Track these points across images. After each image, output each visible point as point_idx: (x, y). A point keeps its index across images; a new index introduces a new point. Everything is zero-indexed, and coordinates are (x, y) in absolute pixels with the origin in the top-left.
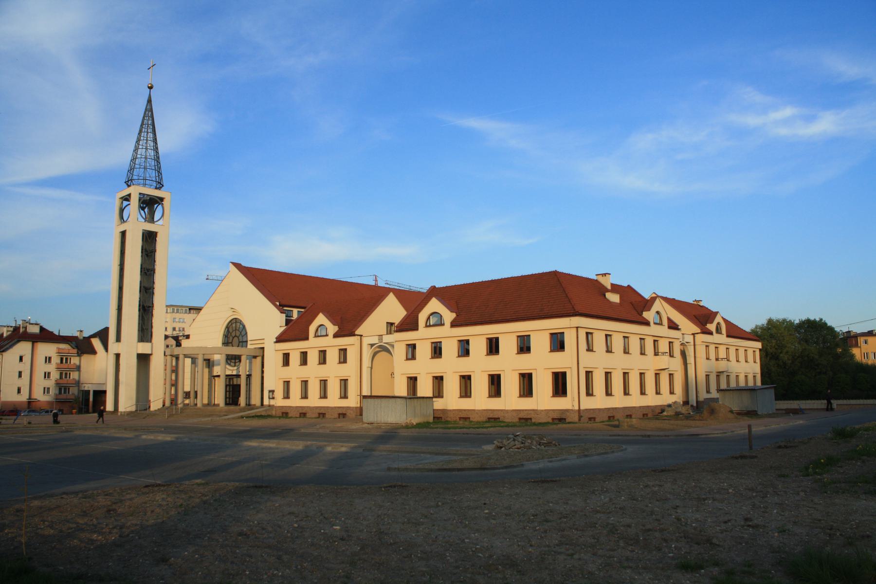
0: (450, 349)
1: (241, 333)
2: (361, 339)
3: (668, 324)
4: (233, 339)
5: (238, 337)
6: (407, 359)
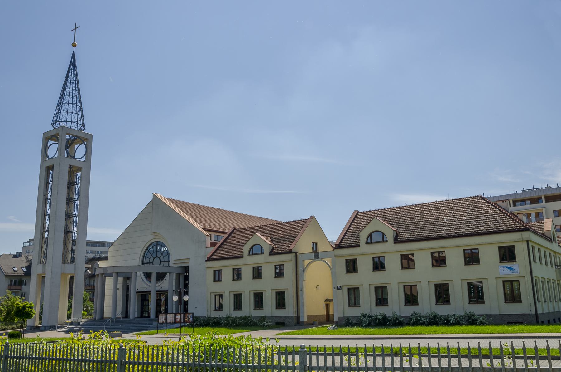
0: (268, 272)
1: (162, 254)
2: (521, 241)
3: (30, 279)
4: (154, 260)
5: (159, 258)
6: (234, 280)
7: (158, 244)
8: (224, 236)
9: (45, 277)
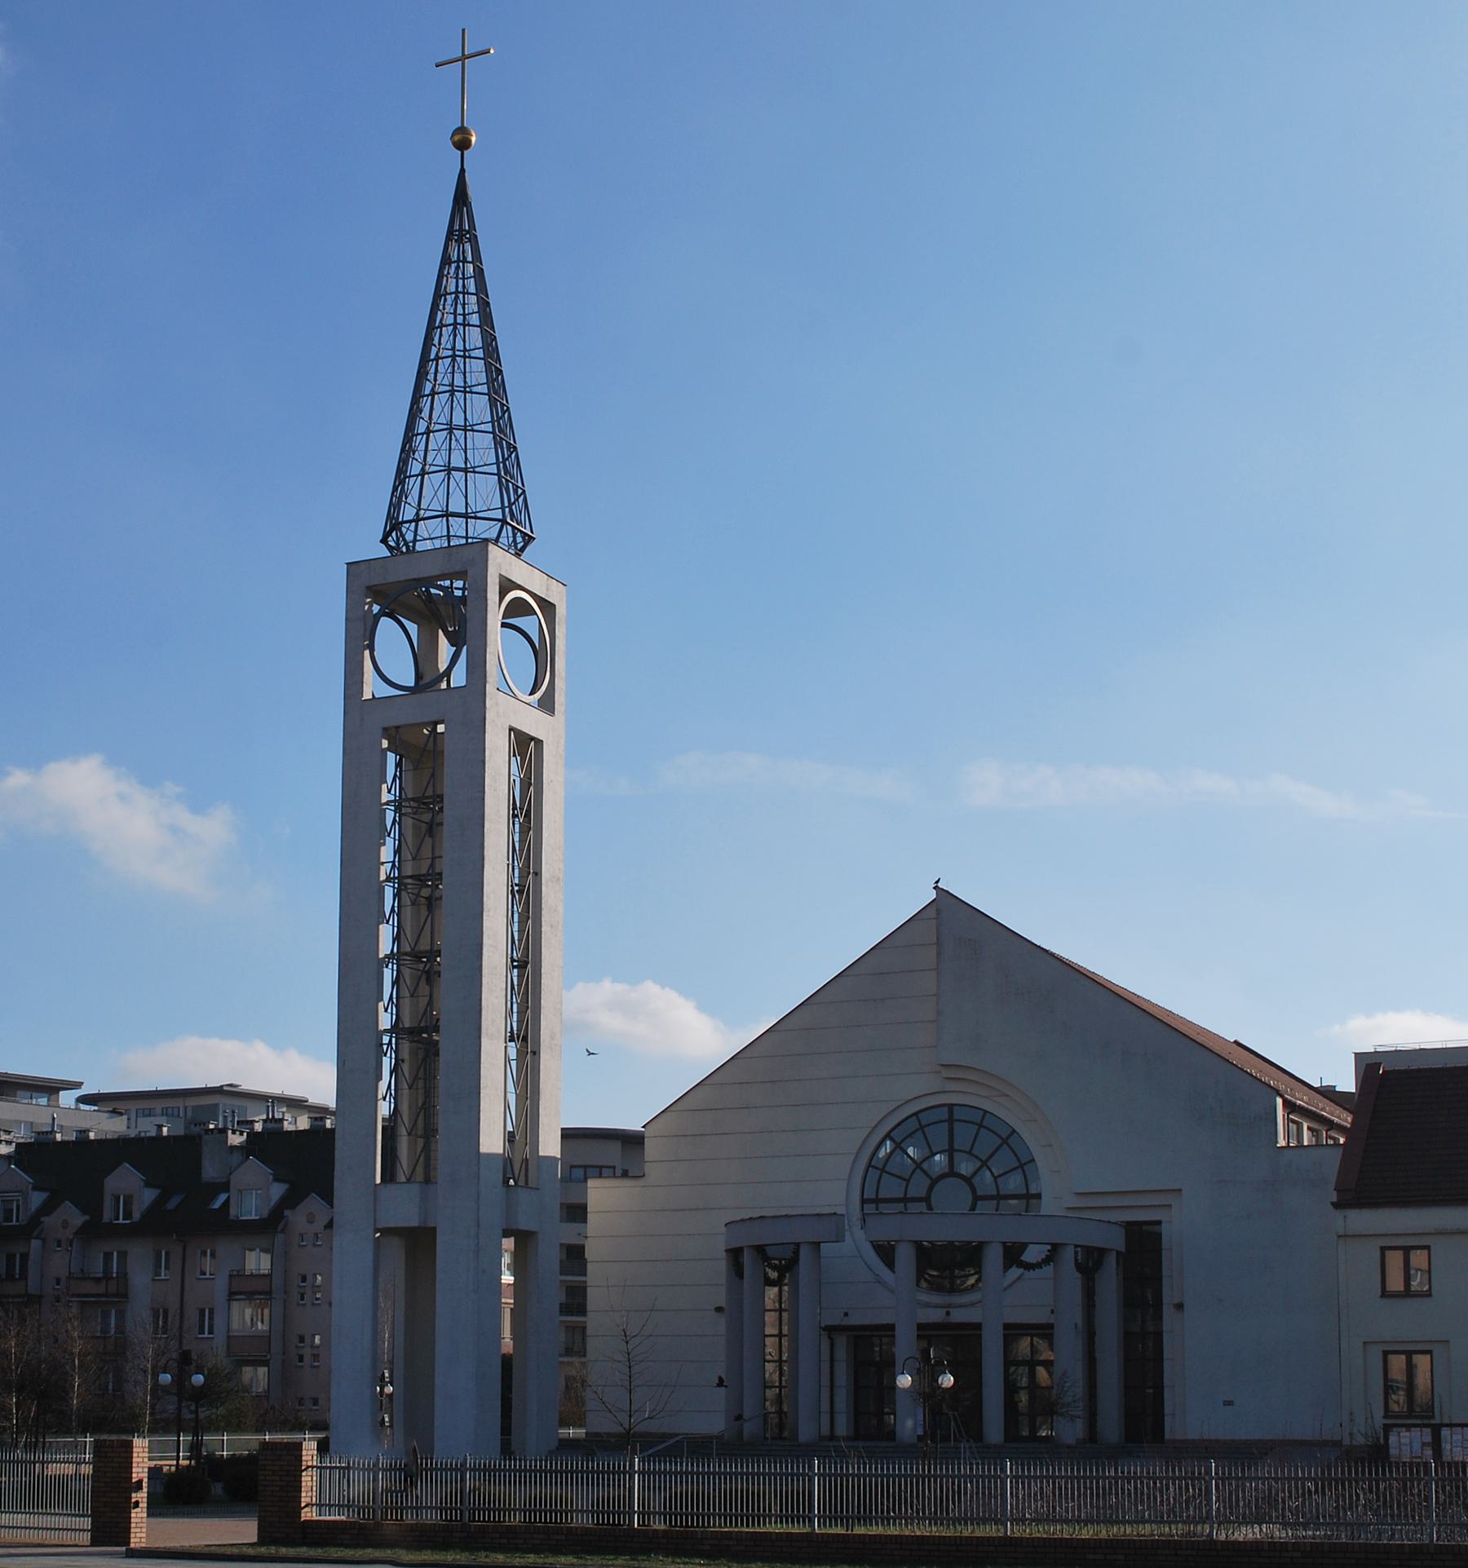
7: (956, 1116)
8: (265, 1322)
9: (318, 1355)
